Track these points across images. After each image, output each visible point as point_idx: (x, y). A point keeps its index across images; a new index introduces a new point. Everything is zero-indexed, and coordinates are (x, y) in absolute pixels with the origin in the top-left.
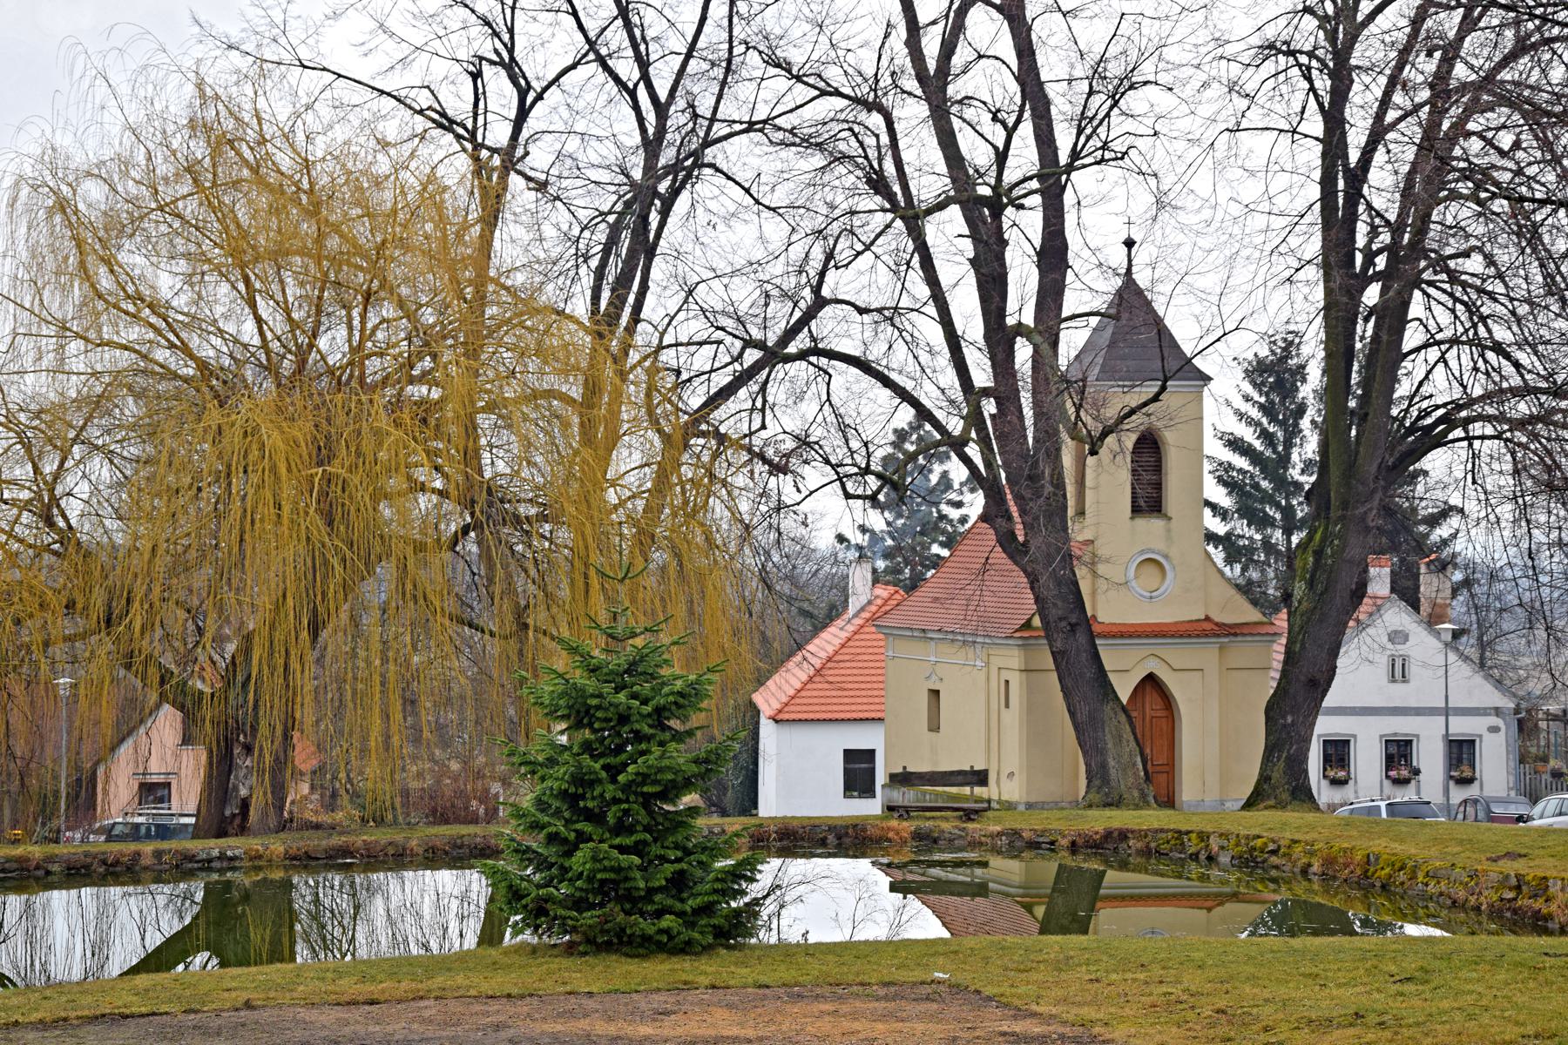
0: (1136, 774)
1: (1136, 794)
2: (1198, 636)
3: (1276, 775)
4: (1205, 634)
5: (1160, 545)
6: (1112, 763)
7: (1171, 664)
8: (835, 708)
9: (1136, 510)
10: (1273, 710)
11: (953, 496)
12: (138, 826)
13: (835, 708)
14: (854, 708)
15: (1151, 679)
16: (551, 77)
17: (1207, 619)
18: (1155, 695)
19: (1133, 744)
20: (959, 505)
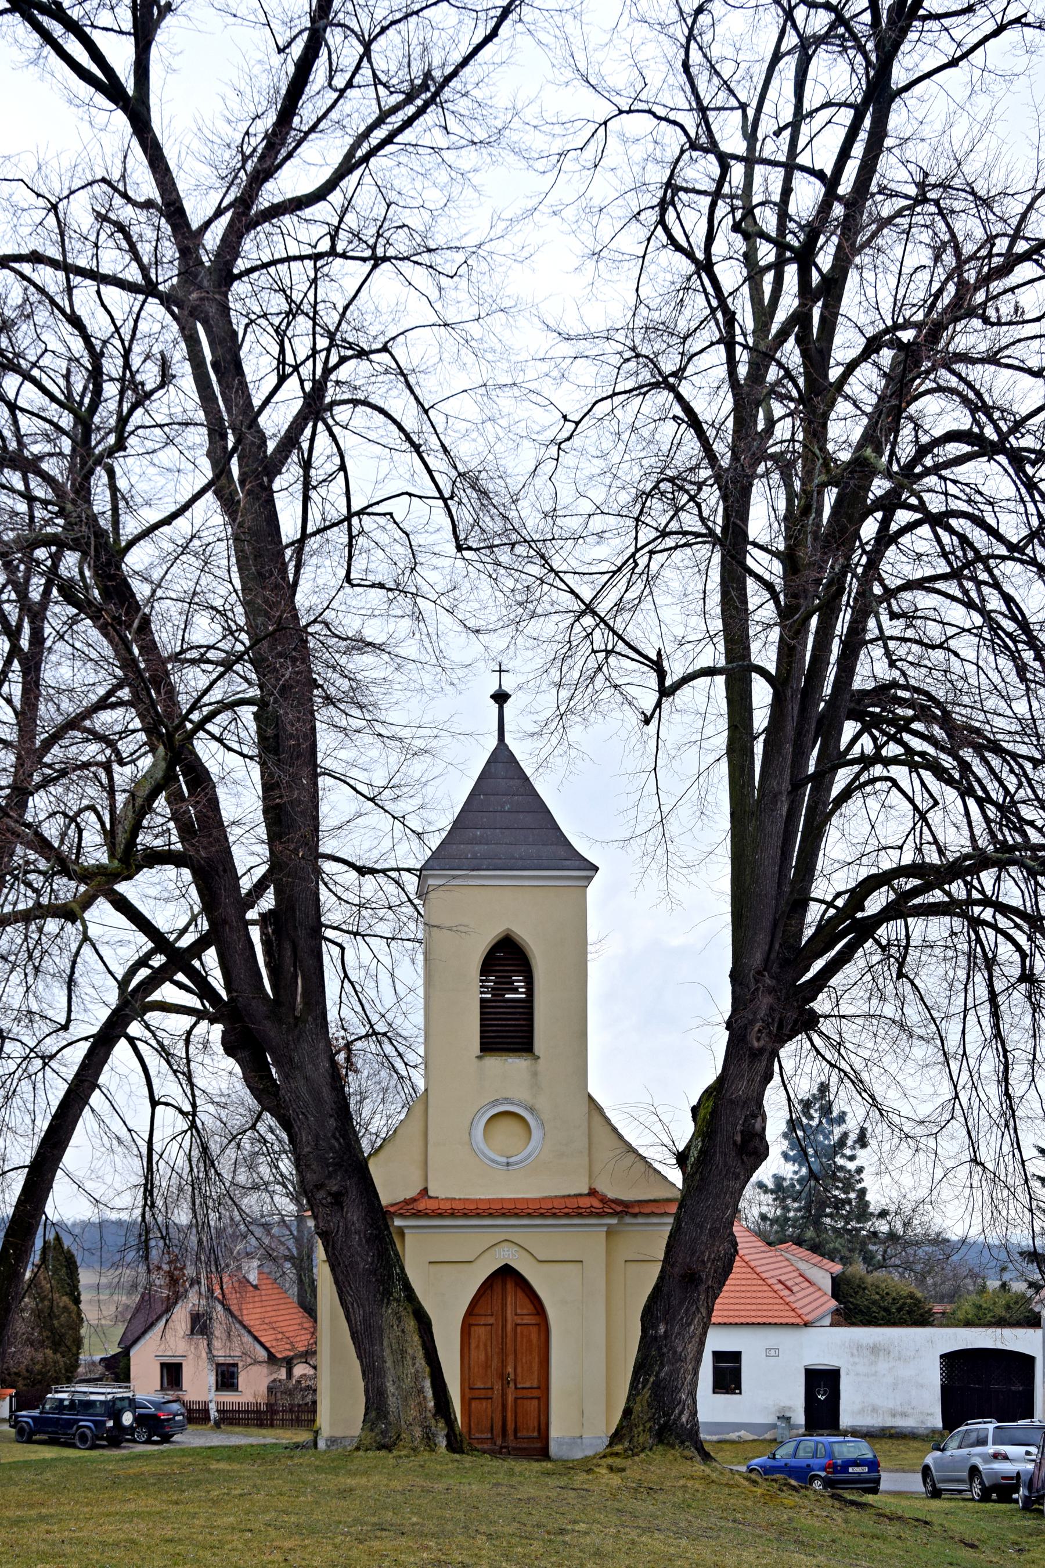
0: (422, 1406)
1: (418, 1433)
2: (567, 1215)
3: (637, 1408)
4: (579, 1213)
5: (522, 1094)
6: (391, 1388)
8: (732, 1313)
11: (848, 1152)
12: (62, 1400)
13: (732, 1313)
14: (770, 1313)
15: (506, 1274)
17: (593, 1193)
18: (520, 1295)
19: (421, 1362)
20: (852, 1158)
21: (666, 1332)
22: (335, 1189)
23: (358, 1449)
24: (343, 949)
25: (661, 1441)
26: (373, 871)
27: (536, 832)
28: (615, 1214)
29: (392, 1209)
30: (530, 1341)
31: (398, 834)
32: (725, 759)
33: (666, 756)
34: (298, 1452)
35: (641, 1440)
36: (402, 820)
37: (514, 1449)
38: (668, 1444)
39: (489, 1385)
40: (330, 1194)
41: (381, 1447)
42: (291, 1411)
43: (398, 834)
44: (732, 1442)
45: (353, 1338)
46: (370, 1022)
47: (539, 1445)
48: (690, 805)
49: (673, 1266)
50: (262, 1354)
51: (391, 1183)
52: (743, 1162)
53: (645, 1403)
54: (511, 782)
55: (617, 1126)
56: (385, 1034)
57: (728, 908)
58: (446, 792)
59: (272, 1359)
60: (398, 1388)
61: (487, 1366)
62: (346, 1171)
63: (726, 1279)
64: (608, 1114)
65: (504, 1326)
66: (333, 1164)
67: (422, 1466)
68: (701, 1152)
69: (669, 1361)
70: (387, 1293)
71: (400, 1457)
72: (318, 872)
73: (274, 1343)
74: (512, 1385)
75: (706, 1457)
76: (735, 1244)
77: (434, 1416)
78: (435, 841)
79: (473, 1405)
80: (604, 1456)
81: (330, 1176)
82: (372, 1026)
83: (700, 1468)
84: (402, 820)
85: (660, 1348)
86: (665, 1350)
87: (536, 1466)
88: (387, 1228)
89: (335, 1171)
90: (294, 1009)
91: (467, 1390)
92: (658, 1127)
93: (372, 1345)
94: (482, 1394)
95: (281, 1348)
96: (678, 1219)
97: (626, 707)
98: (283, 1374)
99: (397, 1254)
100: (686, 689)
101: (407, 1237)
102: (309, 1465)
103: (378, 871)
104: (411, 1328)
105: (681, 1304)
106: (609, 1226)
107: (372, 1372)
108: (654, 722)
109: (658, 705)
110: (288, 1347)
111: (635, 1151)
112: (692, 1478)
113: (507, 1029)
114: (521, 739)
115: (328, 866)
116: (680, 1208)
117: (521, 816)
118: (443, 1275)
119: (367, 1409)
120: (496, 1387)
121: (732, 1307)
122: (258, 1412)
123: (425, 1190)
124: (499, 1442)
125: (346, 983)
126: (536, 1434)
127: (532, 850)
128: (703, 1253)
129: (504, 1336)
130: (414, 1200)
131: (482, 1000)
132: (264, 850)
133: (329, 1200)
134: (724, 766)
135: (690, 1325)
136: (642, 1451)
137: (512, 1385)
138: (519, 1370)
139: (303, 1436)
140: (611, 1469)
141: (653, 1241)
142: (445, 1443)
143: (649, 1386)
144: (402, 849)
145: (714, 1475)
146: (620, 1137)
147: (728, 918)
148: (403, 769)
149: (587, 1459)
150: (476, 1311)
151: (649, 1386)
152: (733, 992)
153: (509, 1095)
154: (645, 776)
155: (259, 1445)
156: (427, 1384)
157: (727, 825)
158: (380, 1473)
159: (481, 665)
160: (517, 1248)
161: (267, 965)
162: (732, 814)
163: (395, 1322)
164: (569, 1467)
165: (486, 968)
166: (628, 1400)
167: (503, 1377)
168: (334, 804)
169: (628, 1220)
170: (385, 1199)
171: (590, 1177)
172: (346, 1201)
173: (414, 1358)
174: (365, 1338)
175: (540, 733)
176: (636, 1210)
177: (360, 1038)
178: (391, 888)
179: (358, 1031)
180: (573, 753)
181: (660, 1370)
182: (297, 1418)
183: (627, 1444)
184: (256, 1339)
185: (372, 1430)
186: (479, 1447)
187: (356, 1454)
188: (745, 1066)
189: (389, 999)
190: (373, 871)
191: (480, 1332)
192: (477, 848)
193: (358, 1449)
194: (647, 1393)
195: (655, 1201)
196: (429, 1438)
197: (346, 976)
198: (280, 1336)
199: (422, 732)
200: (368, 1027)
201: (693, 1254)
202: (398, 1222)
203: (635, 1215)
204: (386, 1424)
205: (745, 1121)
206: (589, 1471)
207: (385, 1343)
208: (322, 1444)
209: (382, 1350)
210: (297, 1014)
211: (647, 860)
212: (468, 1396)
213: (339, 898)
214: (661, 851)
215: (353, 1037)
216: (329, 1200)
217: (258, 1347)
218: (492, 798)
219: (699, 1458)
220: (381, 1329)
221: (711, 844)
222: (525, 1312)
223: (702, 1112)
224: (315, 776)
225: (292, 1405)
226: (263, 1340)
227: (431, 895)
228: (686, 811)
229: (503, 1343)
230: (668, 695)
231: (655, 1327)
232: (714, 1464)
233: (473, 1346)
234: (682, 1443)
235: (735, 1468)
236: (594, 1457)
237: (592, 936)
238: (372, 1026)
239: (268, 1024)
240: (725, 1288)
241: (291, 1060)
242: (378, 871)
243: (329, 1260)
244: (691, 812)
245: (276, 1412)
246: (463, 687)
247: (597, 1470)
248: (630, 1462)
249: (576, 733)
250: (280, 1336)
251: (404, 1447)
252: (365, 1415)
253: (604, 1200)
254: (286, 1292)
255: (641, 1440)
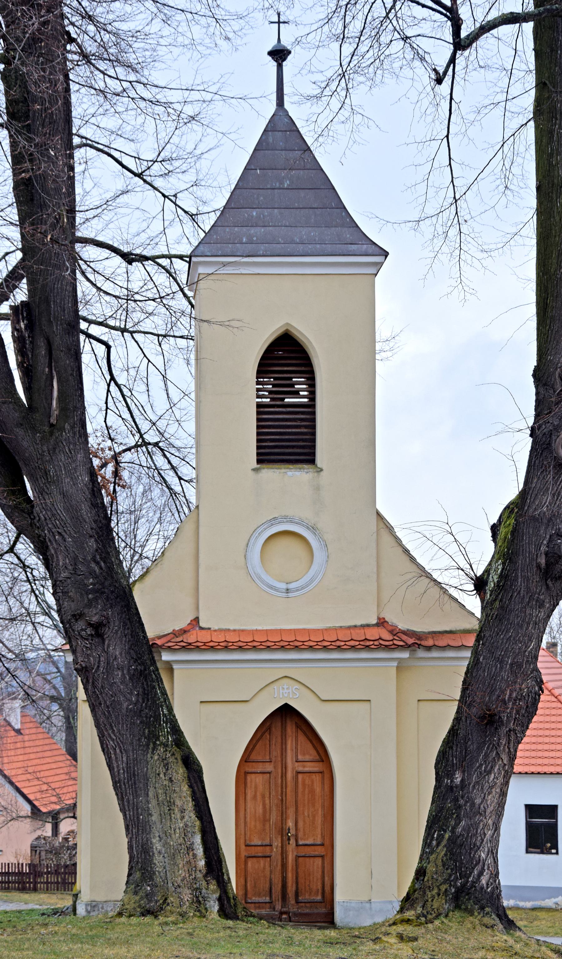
0: (191, 866)
1: (187, 895)
3: (431, 868)
6: (157, 845)
7: (323, 693)
8: (546, 761)
9: (266, 456)
10: (445, 763)
13: (546, 761)
16: (311, 210)
17: (382, 623)
18: (302, 738)
19: (191, 816)
21: (462, 781)
22: (95, 619)
23: (120, 914)
24: (108, 347)
25: (458, 907)
26: (142, 258)
27: (318, 211)
28: (407, 647)
29: (159, 642)
30: (312, 792)
31: (169, 216)
32: (532, 123)
33: (459, 121)
34: (54, 919)
35: (436, 905)
36: (172, 198)
37: (295, 914)
38: (466, 910)
39: (267, 842)
40: (90, 625)
41: (146, 912)
42: (57, 873)
43: (169, 216)
44: (549, 910)
45: (115, 788)
46: (139, 431)
47: (323, 910)
48: (493, 178)
49: (469, 706)
50: (26, 809)
51: (157, 613)
52: (548, 587)
53: (440, 863)
54: (291, 155)
55: (408, 547)
56: (156, 445)
57: (533, 298)
58: (220, 164)
59: (36, 812)
60: (166, 844)
61: (265, 820)
62: (107, 599)
63: (529, 721)
64: (399, 534)
65: (284, 775)
66: (94, 591)
67: (190, 934)
68: (501, 576)
69: (467, 815)
70: (153, 737)
71: (166, 924)
72: (75, 258)
73: (38, 796)
74: (292, 841)
75: (510, 925)
76: (540, 683)
77: (205, 876)
78: (208, 222)
79: (250, 863)
80: (394, 924)
81: (90, 604)
82: (141, 436)
83: (502, 937)
84: (172, 198)
85: (456, 800)
86: (462, 802)
87: (318, 934)
88: (154, 662)
89: (96, 599)
90: (50, 417)
91: (243, 847)
92: (453, 549)
93: (137, 796)
94: (259, 851)
95: (45, 801)
96: (476, 653)
97: (417, 63)
98: (48, 830)
99: (164, 693)
100: (486, 40)
101: (176, 673)
102: (65, 934)
103: (147, 258)
104: (180, 777)
105: (479, 749)
106: (400, 660)
107: (136, 826)
108: (447, 80)
109: (452, 60)
110: (54, 799)
111: (429, 576)
112: (493, 949)
113: (286, 437)
114: (299, 103)
115: (88, 252)
116: (477, 640)
117: (302, 193)
118: (215, 716)
119: (131, 868)
120: (275, 844)
121: (546, 754)
122: (20, 874)
123: (197, 620)
124: (278, 907)
125: (113, 386)
126: (319, 898)
127: (314, 233)
128: (503, 692)
129: (284, 786)
130: (184, 631)
131: (259, 406)
132: (15, 233)
133: (89, 631)
134: (530, 131)
135: (489, 773)
136: (437, 917)
137: (292, 841)
138: (301, 824)
139: (66, 902)
140: (401, 937)
141: (445, 680)
142: (217, 908)
143: (444, 842)
144: (174, 232)
145: (518, 947)
146: (412, 559)
147: (533, 309)
148: (175, 139)
149: (375, 926)
150: (253, 757)
151: (444, 842)
152: (537, 394)
153: (290, 513)
154: (436, 144)
155: (13, 912)
156: (198, 839)
157: (533, 202)
158: (143, 942)
159: (259, 15)
160: (297, 686)
161: (20, 365)
162: (538, 188)
163: (162, 770)
164: (356, 936)
165: (263, 369)
166: (421, 859)
167: (283, 832)
168: (94, 180)
169: (421, 653)
170: (151, 632)
171: (378, 606)
172: (108, 633)
173: (183, 811)
174: (129, 787)
175: (318, 97)
176: (430, 642)
177: (129, 449)
178: (162, 278)
179: (126, 441)
180: (358, 119)
181: (457, 824)
182: (64, 880)
183: (419, 910)
184: (18, 790)
185: (136, 893)
186: (255, 912)
187: (118, 920)
188: (550, 477)
189: (161, 405)
190: (142, 258)
191: (257, 781)
192: (253, 231)
193: (120, 914)
194: (442, 851)
195: (451, 632)
196: (199, 902)
197: (112, 378)
198: (45, 787)
199: (195, 96)
200: (137, 436)
201: (492, 692)
202: (166, 657)
203: (429, 648)
204: (152, 886)
205: (550, 541)
206: (376, 940)
207: (151, 794)
208: (81, 910)
209: (148, 802)
210: (53, 420)
211: (438, 242)
212: (243, 854)
213: (99, 289)
214: (453, 232)
215: (123, 448)
216: (89, 631)
217: (21, 800)
218: (270, 172)
219: (501, 927)
220: (147, 779)
221: (516, 224)
222: (307, 758)
223: (502, 531)
224: (70, 147)
225: (58, 866)
226: (25, 791)
227: (202, 284)
228: (489, 184)
229: (283, 793)
230: (464, 48)
231: (451, 776)
232: (518, 933)
233: (249, 796)
234: (482, 908)
235: (542, 939)
236: (383, 924)
237: (382, 330)
238: (141, 436)
239: (20, 432)
240: (528, 733)
241: (46, 473)
242: (147, 258)
243: (89, 700)
244: (494, 185)
245: (41, 874)
246: (239, 42)
247: (384, 939)
248: (423, 930)
249: (360, 94)
250: (45, 787)
251: (172, 912)
252: (129, 875)
253: (394, 631)
254: (52, 737)
255: (436, 905)
